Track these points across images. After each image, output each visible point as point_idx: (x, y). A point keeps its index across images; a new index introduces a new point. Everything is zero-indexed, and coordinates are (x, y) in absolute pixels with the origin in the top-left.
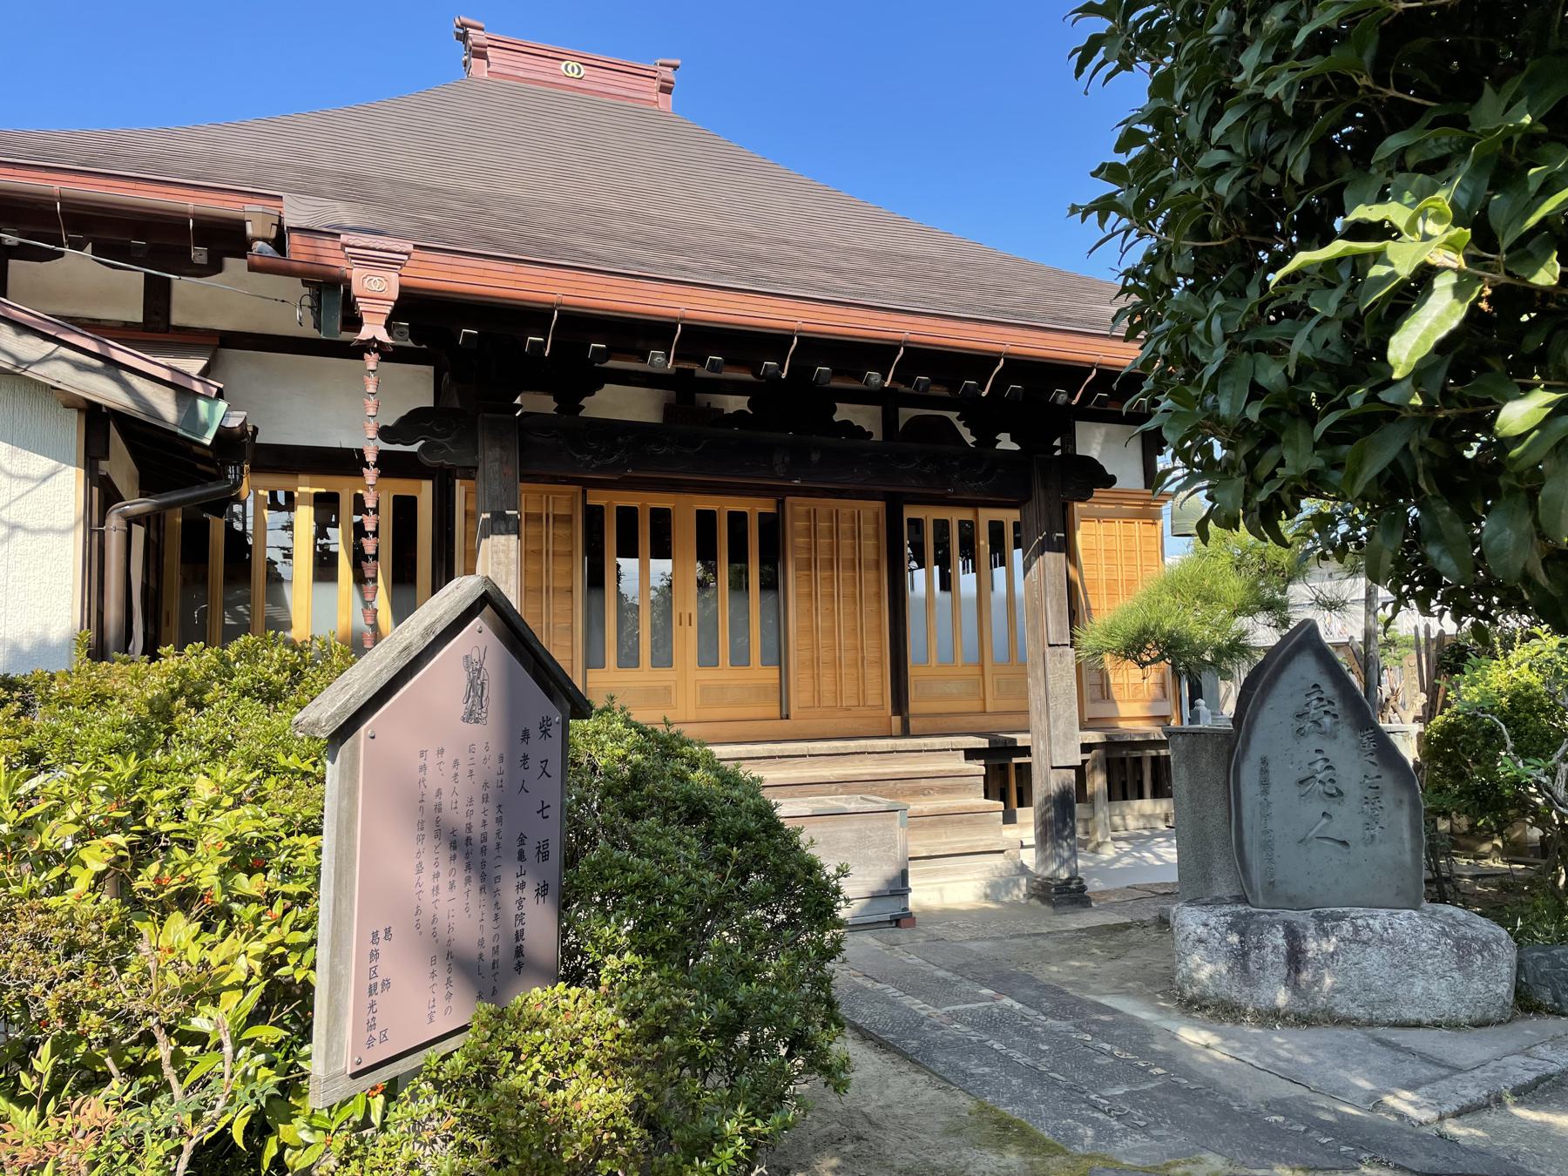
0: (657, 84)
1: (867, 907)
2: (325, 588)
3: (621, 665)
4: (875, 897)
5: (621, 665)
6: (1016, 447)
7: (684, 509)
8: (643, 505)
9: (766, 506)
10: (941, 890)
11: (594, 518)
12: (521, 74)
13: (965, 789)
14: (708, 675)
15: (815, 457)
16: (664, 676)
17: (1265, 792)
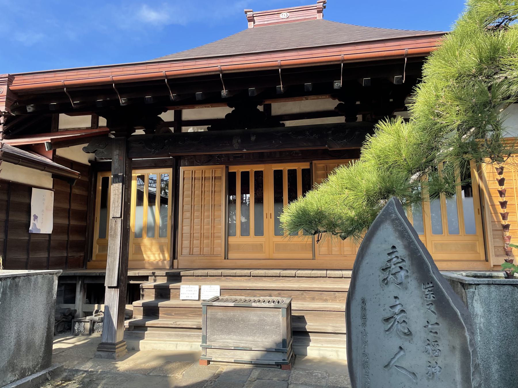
0: (316, 11)
1: (263, 356)
2: (139, 208)
3: (256, 235)
4: (268, 351)
5: (256, 235)
6: (234, 109)
7: (268, 170)
8: (252, 170)
9: (306, 166)
10: (337, 352)
11: (231, 178)
12: (266, 23)
13: (334, 299)
14: (278, 239)
15: (253, 138)
16: (259, 239)
17: (364, 324)
